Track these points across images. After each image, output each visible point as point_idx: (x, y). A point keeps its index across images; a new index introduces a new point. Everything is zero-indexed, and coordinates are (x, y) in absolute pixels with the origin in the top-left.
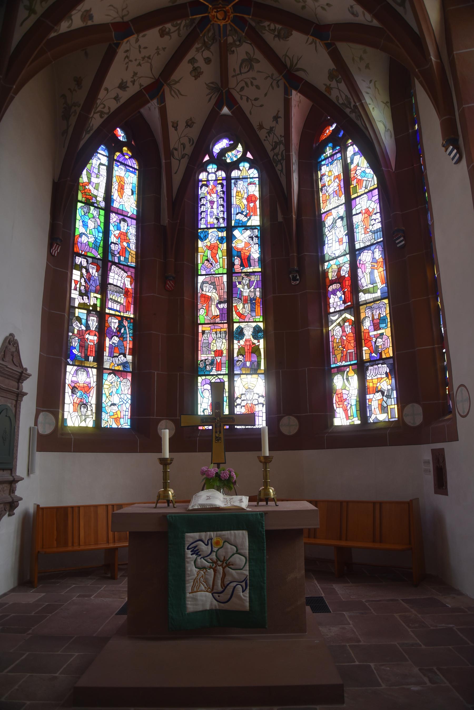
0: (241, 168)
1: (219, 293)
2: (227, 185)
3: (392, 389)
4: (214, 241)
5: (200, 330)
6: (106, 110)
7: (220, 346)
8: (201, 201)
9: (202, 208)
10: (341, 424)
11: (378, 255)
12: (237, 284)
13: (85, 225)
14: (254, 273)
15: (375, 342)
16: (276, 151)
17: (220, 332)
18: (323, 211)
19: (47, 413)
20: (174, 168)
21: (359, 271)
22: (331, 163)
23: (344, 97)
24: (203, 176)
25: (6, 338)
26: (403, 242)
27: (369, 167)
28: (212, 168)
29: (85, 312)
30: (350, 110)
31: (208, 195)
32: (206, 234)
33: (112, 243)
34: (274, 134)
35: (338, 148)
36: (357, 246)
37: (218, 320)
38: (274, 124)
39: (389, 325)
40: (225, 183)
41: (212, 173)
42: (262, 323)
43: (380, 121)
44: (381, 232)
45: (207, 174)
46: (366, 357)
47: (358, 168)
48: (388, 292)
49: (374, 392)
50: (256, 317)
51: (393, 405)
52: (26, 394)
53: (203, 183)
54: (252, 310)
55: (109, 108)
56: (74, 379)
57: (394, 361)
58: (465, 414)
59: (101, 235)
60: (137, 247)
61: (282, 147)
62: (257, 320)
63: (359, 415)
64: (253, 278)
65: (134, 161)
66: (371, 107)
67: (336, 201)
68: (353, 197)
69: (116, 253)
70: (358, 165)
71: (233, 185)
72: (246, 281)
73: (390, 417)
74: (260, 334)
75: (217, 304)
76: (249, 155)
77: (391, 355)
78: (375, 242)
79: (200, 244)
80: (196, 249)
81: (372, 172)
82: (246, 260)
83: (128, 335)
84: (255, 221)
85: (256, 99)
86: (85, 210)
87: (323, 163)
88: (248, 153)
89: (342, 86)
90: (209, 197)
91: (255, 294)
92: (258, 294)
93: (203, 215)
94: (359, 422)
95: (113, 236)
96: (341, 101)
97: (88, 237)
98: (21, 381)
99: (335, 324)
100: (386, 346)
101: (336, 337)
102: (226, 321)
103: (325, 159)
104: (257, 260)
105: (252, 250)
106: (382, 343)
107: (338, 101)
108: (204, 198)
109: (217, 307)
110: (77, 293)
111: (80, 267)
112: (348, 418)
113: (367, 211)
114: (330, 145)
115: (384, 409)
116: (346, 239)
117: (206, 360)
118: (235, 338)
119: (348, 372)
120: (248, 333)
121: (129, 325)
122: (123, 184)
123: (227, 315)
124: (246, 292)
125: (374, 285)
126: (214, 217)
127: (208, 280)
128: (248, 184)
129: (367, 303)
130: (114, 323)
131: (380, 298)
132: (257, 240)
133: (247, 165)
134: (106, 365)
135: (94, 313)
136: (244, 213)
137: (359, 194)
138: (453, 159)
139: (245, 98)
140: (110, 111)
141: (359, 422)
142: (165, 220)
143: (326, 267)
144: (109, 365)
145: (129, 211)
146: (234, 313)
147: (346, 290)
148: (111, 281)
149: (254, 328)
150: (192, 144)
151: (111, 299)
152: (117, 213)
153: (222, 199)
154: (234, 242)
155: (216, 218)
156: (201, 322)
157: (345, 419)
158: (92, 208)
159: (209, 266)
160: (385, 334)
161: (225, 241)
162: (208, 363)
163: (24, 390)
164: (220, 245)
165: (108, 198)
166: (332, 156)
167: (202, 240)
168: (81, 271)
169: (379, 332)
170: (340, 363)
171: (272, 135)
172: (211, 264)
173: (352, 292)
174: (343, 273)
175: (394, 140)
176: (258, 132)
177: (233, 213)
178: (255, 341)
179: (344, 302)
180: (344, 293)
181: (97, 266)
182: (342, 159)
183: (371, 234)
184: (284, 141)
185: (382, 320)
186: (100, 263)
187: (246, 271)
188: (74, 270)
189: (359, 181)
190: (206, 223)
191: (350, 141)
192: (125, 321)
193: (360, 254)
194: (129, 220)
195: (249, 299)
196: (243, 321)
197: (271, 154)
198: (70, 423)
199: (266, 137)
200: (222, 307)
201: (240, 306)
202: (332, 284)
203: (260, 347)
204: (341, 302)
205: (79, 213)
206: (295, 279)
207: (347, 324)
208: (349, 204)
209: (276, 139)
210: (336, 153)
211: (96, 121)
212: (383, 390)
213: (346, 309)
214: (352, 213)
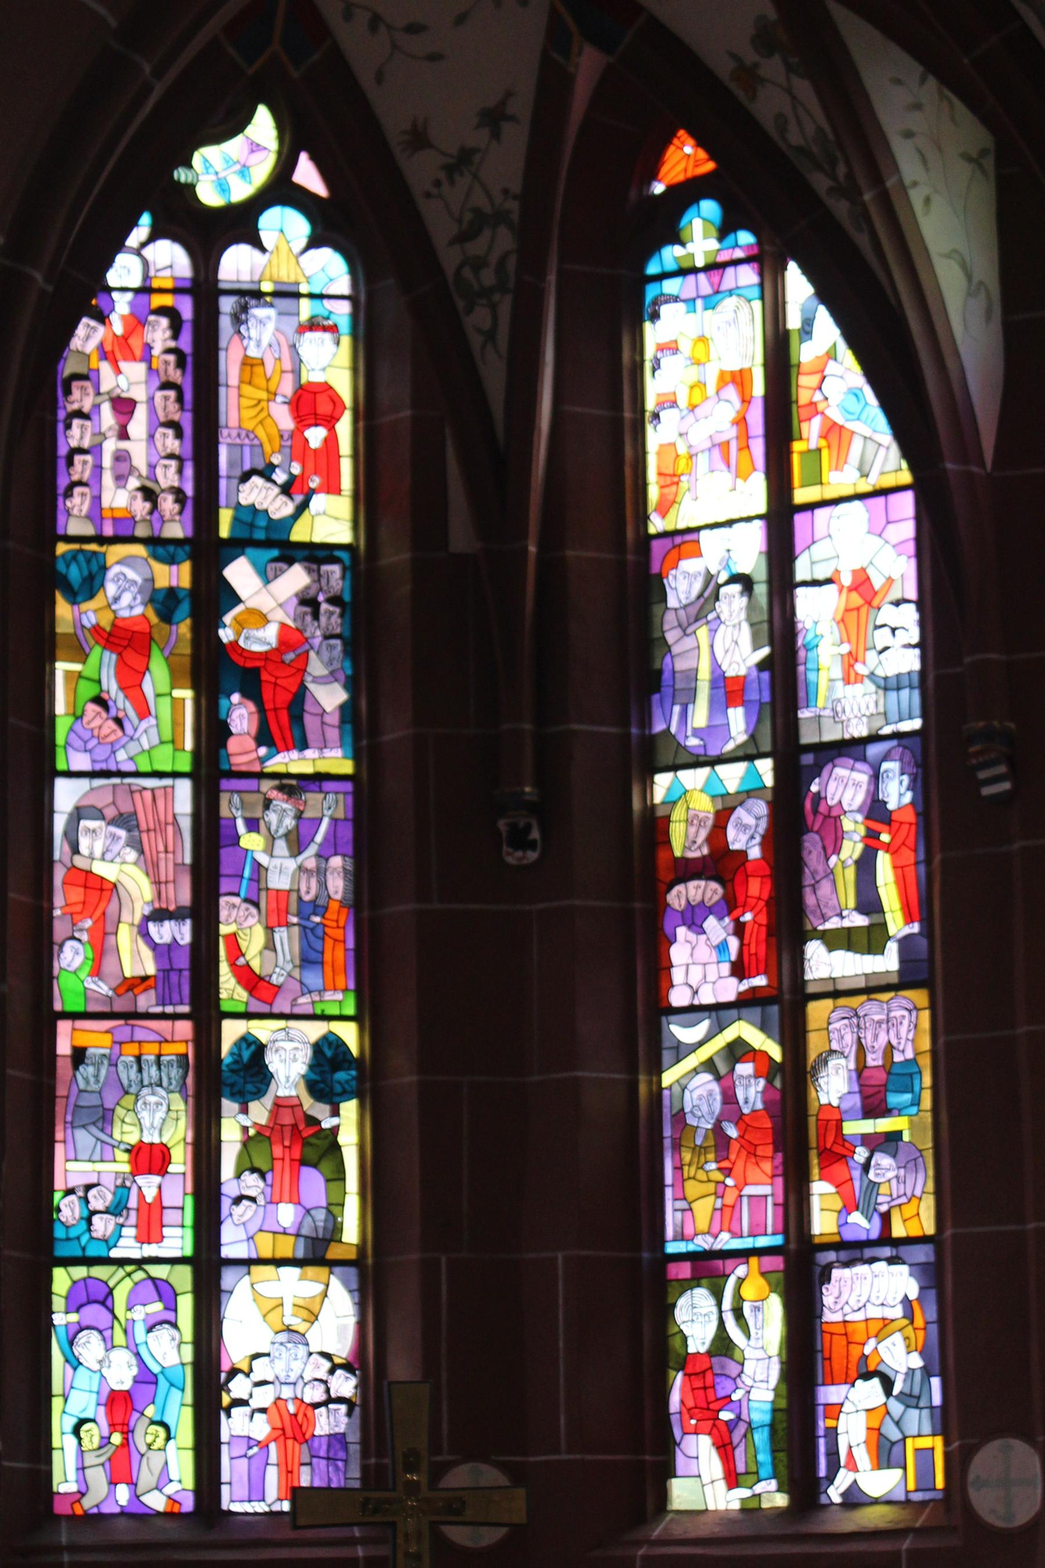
0: (267, 237)
1: (156, 865)
2: (203, 312)
3: (927, 1372)
5: (64, 1047)
7: (157, 1122)
8: (68, 392)
14: (319, 779)
15: (866, 1167)
16: (477, 247)
17: (159, 1056)
18: (656, 525)
21: (811, 843)
22: (711, 300)
26: (1006, 786)
30: (831, 183)
31: (105, 368)
32: (95, 568)
34: (475, 176)
37: (146, 1001)
38: (480, 138)
39: (927, 1102)
40: (186, 308)
43: (948, 256)
44: (916, 693)
46: (823, 1223)
49: (853, 1374)
50: (328, 996)
51: (924, 1439)
54: (307, 960)
57: (939, 1253)
61: (505, 240)
62: (334, 1010)
63: (783, 1470)
64: (315, 802)
66: (916, 197)
71: (225, 323)
72: (281, 816)
73: (911, 1486)
74: (341, 1076)
75: (146, 919)
76: (307, 175)
77: (930, 1229)
82: (284, 716)
84: (331, 520)
85: (414, 29)
87: (670, 286)
88: (304, 159)
91: (323, 885)
92: (337, 886)
93: (82, 467)
94: (781, 1500)
96: (794, 138)
101: (691, 1121)
102: (185, 1009)
103: (683, 272)
104: (334, 719)
107: (783, 129)
108: (84, 377)
109: (144, 933)
112: (732, 1479)
113: (862, 583)
114: (710, 208)
117: (88, 1187)
118: (226, 1090)
119: (741, 1281)
120: (289, 1067)
123: (195, 976)
124: (282, 872)
126: (133, 483)
127: (102, 800)
128: (300, 309)
129: (836, 994)
131: (894, 979)
132: (335, 620)
136: (280, 477)
137: (830, 494)
141: (781, 1500)
146: (224, 968)
149: (317, 1048)
153: (172, 394)
154: (228, 619)
156: (70, 1007)
157: (722, 1485)
159: (105, 731)
160: (906, 1137)
161: (185, 607)
162: (96, 1204)
166: (714, 267)
167: (73, 597)
170: (710, 1239)
171: (463, 182)
172: (119, 722)
173: (772, 931)
174: (736, 839)
178: (320, 1111)
179: (739, 970)
180: (739, 930)
182: (762, 298)
183: (872, 688)
184: (515, 217)
187: (281, 769)
190: (96, 512)
193: (816, 771)
195: (293, 907)
196: (265, 1008)
197: (450, 258)
200: (167, 939)
201: (253, 943)
202: (684, 879)
203: (341, 1140)
204: (726, 968)
206: (519, 840)
207: (744, 1069)
208: (782, 520)
209: (479, 199)
210: (736, 263)
213: (745, 1002)
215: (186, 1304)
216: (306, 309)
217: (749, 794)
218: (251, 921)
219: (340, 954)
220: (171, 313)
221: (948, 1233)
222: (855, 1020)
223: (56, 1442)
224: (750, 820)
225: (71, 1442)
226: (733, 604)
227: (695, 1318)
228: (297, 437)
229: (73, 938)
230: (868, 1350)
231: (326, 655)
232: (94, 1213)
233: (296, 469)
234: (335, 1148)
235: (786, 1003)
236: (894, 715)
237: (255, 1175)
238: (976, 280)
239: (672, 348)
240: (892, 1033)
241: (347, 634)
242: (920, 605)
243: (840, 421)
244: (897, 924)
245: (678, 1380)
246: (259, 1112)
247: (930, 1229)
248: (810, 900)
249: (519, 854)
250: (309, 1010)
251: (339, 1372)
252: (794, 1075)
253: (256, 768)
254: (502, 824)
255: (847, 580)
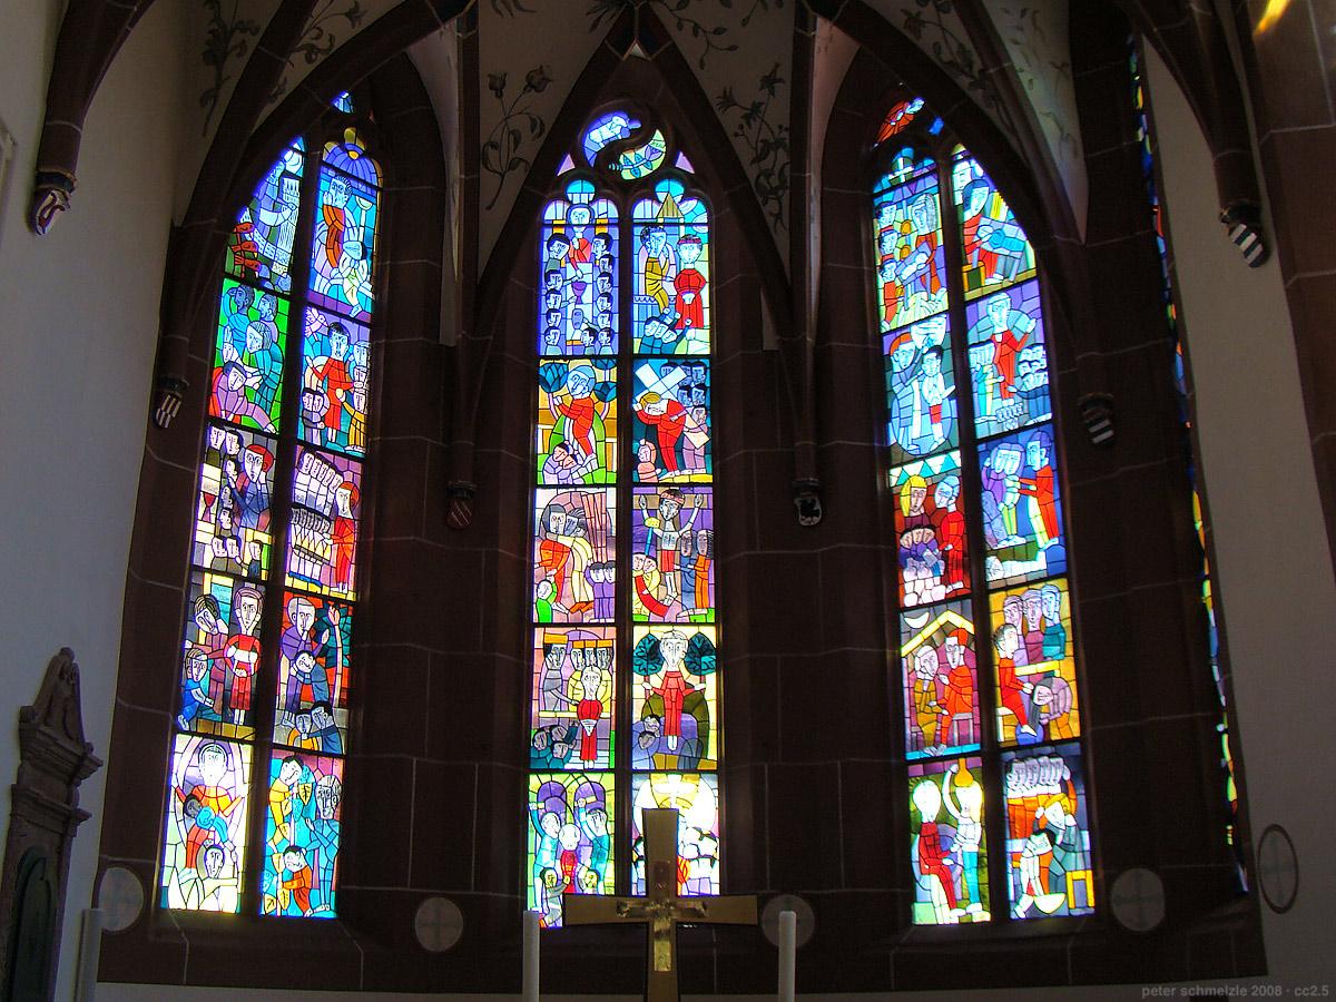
0: (661, 197)
4: (581, 392)
5: (538, 644)
6: (323, 43)
8: (547, 280)
9: (552, 300)
10: (935, 922)
11: (1039, 458)
12: (646, 515)
13: (239, 340)
15: (1032, 696)
16: (766, 164)
18: (885, 327)
19: (124, 870)
20: (485, 199)
21: (987, 497)
23: (955, 48)
24: (554, 212)
25: (55, 661)
26: (1109, 434)
27: (1014, 222)
28: (580, 191)
29: (229, 581)
31: (569, 266)
32: (561, 373)
33: (309, 390)
35: (928, 162)
36: (981, 432)
40: (615, 233)
41: (581, 205)
42: (713, 629)
43: (1048, 115)
45: (567, 207)
46: (1005, 734)
47: (983, 221)
48: (1067, 560)
50: (698, 611)
51: (1080, 874)
52: (86, 816)
53: (556, 231)
55: (332, 38)
56: (192, 773)
57: (1083, 749)
58: (1285, 902)
59: (278, 368)
60: (370, 405)
61: (782, 156)
64: (689, 501)
65: (370, 164)
66: (1024, 78)
67: (925, 304)
68: (969, 296)
69: (316, 418)
70: (982, 213)
71: (637, 241)
72: (669, 508)
73: (1071, 905)
74: (705, 659)
76: (683, 163)
78: (1031, 422)
79: (543, 399)
80: (531, 414)
81: (1021, 236)
83: (340, 651)
84: (698, 342)
85: (718, 31)
86: (241, 299)
87: (887, 197)
89: (952, 20)
90: (571, 272)
94: (987, 917)
95: (309, 372)
96: (946, 57)
97: (244, 373)
98: (76, 780)
99: (918, 639)
100: (1061, 705)
102: (613, 621)
103: (895, 187)
105: (689, 423)
106: (1049, 699)
108: (558, 272)
110: (211, 528)
111: (221, 458)
112: (952, 902)
114: (907, 151)
115: (1051, 882)
116: (950, 409)
117: (552, 727)
120: (674, 657)
121: (343, 620)
122: (342, 228)
125: (1029, 538)
126: (584, 326)
128: (680, 241)
129: (1007, 588)
130: (302, 615)
131: (1044, 574)
133: (677, 189)
134: (279, 737)
135: (253, 586)
138: (1247, 252)
139: (688, 27)
140: (332, 45)
141: (987, 917)
142: (451, 329)
143: (893, 481)
144: (285, 735)
145: (354, 301)
146: (635, 596)
147: (950, 547)
148: (299, 494)
150: (540, 134)
151: (299, 548)
152: (321, 309)
154: (638, 398)
155: (589, 329)
158: (259, 294)
160: (1057, 674)
161: (613, 393)
163: (83, 805)
164: (599, 406)
165: (301, 266)
166: (911, 181)
168: (223, 467)
169: (1042, 667)
170: (934, 749)
171: (755, 125)
172: (574, 456)
174: (941, 501)
175: (1083, 162)
176: (719, 114)
177: (636, 318)
178: (694, 680)
179: (945, 581)
181: (266, 453)
182: (939, 192)
184: (787, 142)
185: (1050, 634)
186: (273, 445)
187: (670, 481)
188: (205, 465)
189: (988, 258)
191: (962, 149)
192: (332, 610)
193: (988, 452)
194: (352, 328)
197: (752, 172)
198: (175, 901)
199: (741, 127)
201: (652, 582)
204: (937, 579)
205: (227, 305)
206: (808, 510)
207: (952, 641)
209: (765, 135)
210: (923, 176)
211: (296, 70)
212: (1053, 830)
213: (949, 600)
214: (966, 340)
215: (610, 799)
216: (683, 231)
217: (947, 473)
218: (652, 569)
219: (705, 584)
220: (607, 237)
221: (1089, 730)
222: (1020, 603)
223: (530, 882)
224: (947, 488)
225: (539, 882)
226: (932, 364)
227: (926, 800)
228: (679, 298)
229: (546, 580)
230: (1038, 815)
231: (695, 417)
232: (554, 742)
233: (678, 316)
234: (702, 702)
235: (977, 598)
236: (1034, 413)
237: (654, 719)
238: (1066, 132)
239: (890, 229)
240: (1044, 609)
241: (708, 404)
242: (1046, 346)
243: (990, 249)
244: (1043, 540)
245: (916, 839)
246: (656, 681)
247: (1076, 732)
248: (988, 531)
249: (809, 519)
250: (687, 620)
251: (705, 838)
252: (983, 641)
253: (655, 480)
254: (797, 501)
255: (999, 338)
